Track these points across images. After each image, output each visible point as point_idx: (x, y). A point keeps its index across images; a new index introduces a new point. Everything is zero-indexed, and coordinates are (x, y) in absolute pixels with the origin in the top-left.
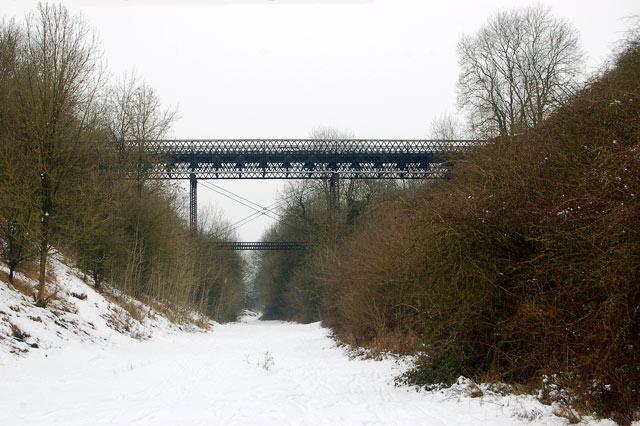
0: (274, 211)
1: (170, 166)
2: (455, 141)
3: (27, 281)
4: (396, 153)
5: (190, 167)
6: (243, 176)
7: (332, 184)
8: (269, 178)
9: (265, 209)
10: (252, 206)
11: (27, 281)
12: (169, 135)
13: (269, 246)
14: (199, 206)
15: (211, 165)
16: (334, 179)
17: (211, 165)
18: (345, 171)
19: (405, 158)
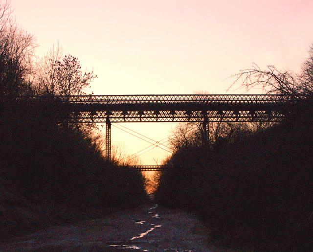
0: (166, 144)
1: (93, 113)
2: (83, 96)
3: (147, 232)
4: (236, 104)
5: (122, 114)
6: (127, 121)
7: (204, 126)
8: (161, 121)
9: (157, 142)
10: (148, 140)
11: (147, 232)
12: (86, 90)
13: (167, 170)
14: (112, 144)
15: (137, 112)
16: (206, 122)
17: (137, 112)
18: (213, 115)
19: (252, 107)
